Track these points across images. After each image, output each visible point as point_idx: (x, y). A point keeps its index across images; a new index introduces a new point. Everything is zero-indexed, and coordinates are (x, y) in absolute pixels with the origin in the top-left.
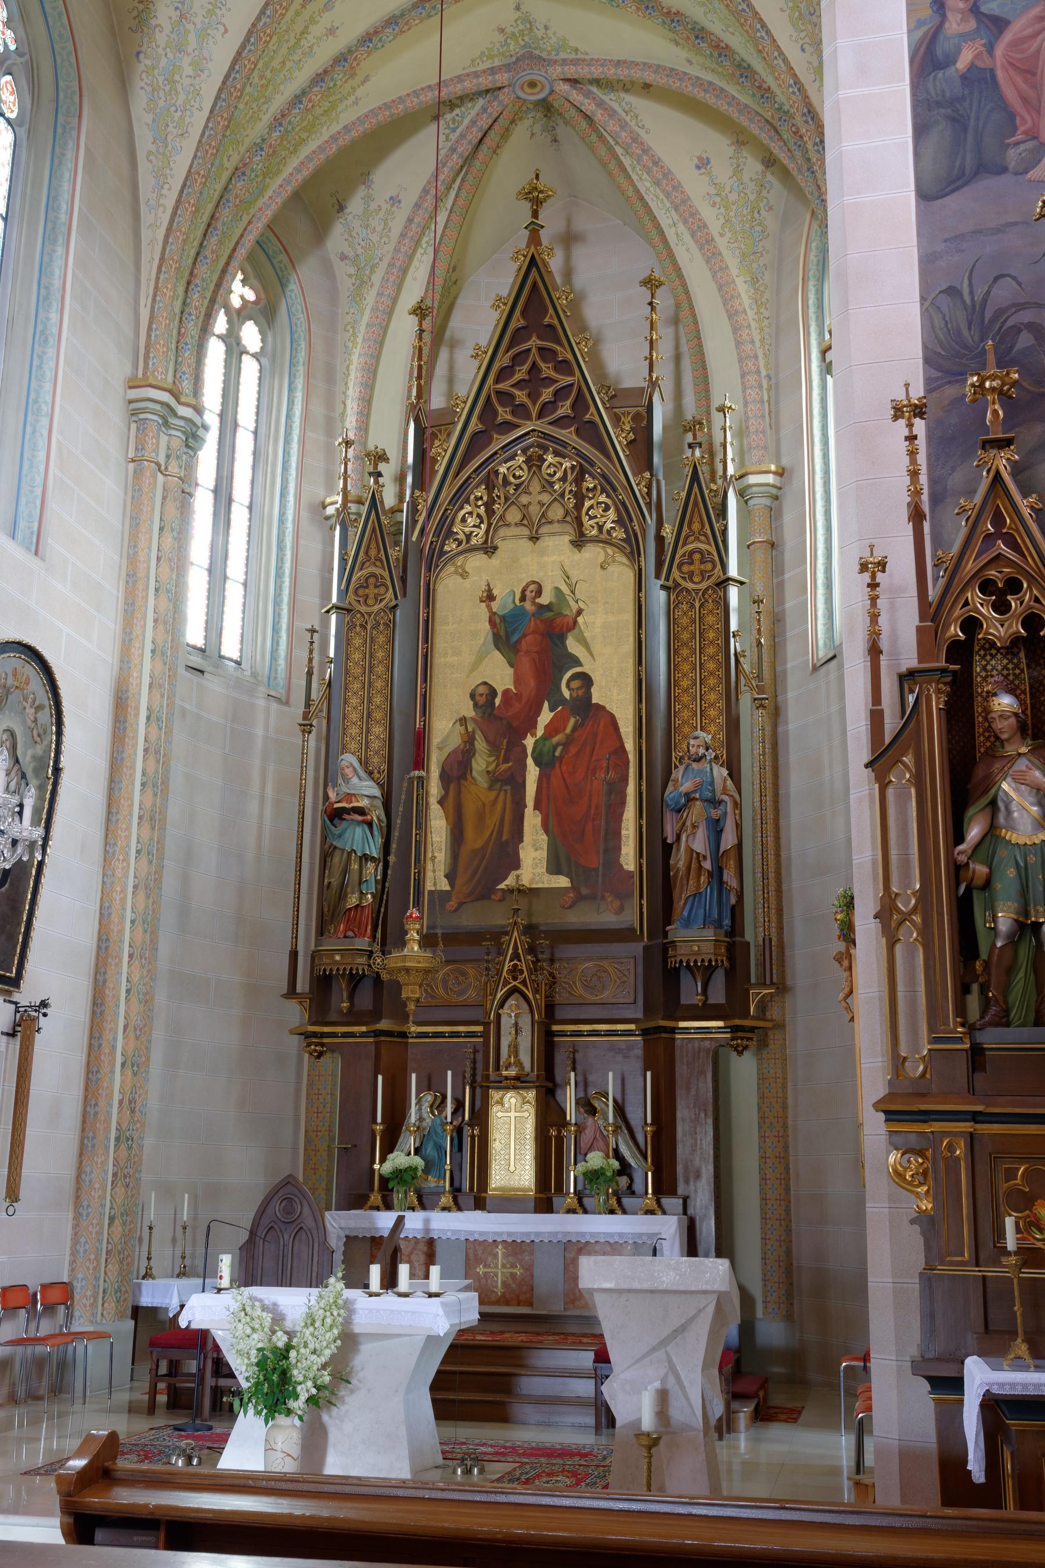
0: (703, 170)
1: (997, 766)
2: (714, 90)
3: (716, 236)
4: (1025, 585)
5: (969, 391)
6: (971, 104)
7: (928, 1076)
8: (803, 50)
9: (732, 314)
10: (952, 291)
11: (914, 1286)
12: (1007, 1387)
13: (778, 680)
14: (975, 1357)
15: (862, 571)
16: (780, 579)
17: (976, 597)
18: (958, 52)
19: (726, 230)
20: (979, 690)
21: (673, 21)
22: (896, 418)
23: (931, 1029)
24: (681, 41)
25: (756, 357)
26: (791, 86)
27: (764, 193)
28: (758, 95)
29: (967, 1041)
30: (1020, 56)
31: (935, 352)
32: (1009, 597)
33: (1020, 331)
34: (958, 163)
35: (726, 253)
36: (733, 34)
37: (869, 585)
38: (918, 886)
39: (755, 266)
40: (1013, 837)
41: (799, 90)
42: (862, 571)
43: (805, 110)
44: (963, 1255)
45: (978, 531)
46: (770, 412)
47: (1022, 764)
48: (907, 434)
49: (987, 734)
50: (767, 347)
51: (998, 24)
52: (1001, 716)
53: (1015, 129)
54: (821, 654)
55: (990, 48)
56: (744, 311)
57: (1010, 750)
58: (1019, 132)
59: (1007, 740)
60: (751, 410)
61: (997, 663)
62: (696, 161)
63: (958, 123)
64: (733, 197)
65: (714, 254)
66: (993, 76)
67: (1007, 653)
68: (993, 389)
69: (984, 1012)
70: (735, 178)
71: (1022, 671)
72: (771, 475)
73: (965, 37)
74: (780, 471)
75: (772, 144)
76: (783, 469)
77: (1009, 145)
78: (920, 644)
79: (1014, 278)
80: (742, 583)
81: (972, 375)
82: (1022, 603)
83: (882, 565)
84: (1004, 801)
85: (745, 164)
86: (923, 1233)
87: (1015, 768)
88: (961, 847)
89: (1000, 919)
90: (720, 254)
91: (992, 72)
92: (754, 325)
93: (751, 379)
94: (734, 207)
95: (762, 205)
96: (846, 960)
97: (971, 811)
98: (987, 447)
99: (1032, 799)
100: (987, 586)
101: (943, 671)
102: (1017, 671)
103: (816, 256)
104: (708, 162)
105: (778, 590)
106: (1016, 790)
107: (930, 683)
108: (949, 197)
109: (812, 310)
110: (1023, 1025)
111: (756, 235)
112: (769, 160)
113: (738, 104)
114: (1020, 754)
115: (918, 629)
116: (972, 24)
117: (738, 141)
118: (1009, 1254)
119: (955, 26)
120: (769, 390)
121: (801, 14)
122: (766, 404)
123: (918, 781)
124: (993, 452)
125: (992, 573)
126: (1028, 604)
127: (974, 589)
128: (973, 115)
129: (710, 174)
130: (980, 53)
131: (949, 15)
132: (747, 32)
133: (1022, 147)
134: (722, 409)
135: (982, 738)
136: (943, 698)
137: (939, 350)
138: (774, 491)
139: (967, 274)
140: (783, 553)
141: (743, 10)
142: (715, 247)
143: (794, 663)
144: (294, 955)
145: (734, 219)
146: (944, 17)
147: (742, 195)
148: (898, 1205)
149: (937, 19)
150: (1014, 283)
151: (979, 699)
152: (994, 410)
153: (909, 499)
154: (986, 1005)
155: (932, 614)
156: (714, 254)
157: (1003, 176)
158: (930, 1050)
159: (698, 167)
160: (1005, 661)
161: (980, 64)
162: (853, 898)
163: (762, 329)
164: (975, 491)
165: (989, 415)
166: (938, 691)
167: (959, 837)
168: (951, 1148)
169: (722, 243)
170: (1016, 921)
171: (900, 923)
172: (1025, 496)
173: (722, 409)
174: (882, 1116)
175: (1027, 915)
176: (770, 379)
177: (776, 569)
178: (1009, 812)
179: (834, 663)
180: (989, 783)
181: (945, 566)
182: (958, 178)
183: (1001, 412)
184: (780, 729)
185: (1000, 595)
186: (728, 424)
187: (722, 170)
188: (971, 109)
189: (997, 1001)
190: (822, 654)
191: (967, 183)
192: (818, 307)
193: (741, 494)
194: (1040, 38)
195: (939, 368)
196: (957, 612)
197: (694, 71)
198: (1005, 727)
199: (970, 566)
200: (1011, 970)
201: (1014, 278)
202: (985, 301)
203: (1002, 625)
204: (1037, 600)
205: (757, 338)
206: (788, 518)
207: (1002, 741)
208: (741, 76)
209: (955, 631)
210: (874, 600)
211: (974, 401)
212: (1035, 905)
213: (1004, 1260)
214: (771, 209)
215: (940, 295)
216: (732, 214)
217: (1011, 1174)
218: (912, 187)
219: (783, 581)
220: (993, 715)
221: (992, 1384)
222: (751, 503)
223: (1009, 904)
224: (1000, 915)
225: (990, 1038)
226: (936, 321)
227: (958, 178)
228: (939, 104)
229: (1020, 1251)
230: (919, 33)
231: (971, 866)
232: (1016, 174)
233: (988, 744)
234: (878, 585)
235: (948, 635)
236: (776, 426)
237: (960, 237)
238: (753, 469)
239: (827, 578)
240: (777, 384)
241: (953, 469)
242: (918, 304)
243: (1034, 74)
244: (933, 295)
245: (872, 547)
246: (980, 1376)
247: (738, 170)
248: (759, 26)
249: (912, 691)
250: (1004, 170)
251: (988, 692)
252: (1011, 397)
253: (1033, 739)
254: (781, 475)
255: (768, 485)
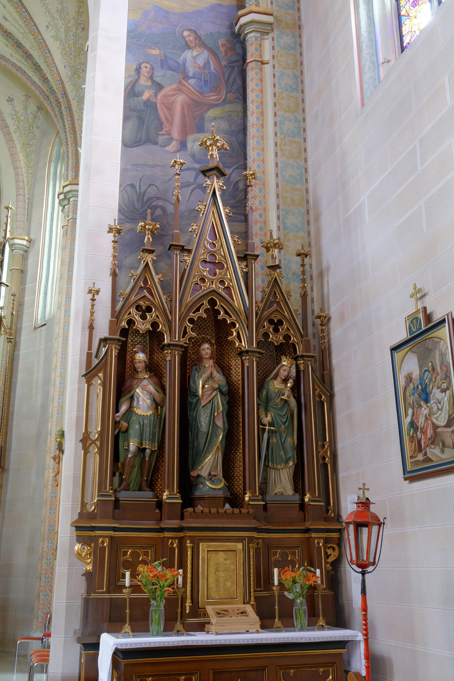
0: (10, 103)
1: (135, 382)
2: (21, 71)
3: (12, 133)
4: (153, 310)
5: (139, 228)
6: (146, 114)
7: (96, 511)
8: (65, 68)
9: (15, 168)
10: (132, 186)
11: (79, 603)
12: (143, 644)
13: (18, 331)
14: (106, 633)
15: (89, 293)
16: (24, 287)
17: (133, 311)
18: (144, 92)
19: (17, 131)
20: (129, 350)
21: (7, 36)
22: (109, 232)
23: (99, 491)
24: (9, 45)
25: (24, 189)
26: (58, 80)
27: (36, 120)
28: (42, 79)
29: (113, 496)
30: (167, 101)
31: (123, 209)
32: (147, 314)
33: (157, 208)
34: (139, 136)
35: (15, 140)
36: (34, 50)
37: (91, 299)
38: (99, 429)
39: (28, 150)
40: (139, 412)
41: (61, 83)
42: (89, 293)
43: (63, 92)
44: (103, 589)
45: (137, 285)
46: (28, 214)
47: (145, 382)
48: (113, 240)
49: (130, 368)
50: (29, 186)
51: (160, 87)
52: (139, 362)
53: (162, 129)
54: (39, 322)
55: (156, 95)
56: (21, 168)
57: (141, 376)
58: (164, 131)
59: (140, 372)
60: (19, 211)
61: (138, 339)
62: (7, 98)
63: (141, 120)
64: (22, 118)
65: (10, 140)
66: (156, 106)
67: (142, 336)
68: (149, 229)
69: (120, 485)
70: (24, 110)
71: (147, 344)
72: (25, 241)
73: (147, 87)
74: (29, 240)
75: (45, 102)
76: (31, 240)
77: (159, 134)
78: (110, 327)
79: (157, 187)
80: (7, 286)
81: (142, 222)
82: (151, 317)
83: (98, 292)
84: (137, 397)
85: (29, 106)
86: (86, 580)
87: (142, 383)
88: (117, 414)
89: (131, 446)
90: (13, 141)
91: (156, 104)
92: (25, 175)
93: (21, 197)
94: (22, 123)
95: (34, 125)
96: (58, 459)
97: (122, 400)
98: (144, 251)
99: (148, 397)
100: (138, 308)
101: (119, 340)
102: (145, 344)
103: (56, 153)
104: (13, 100)
105: (22, 291)
106: (142, 393)
107: (113, 344)
108: (134, 148)
109: (51, 175)
110: (134, 490)
111: (30, 137)
112: (40, 107)
113: (31, 80)
114: (145, 378)
115: (110, 321)
116: (150, 83)
117: (27, 95)
118: (126, 588)
119: (143, 81)
120: (29, 204)
121: (66, 52)
122: (26, 210)
123: (104, 384)
124: (147, 254)
125: (141, 303)
126: (154, 318)
127: (133, 308)
128: (147, 118)
129: (13, 105)
130: (152, 95)
131: (141, 77)
132: (42, 52)
133: (164, 137)
134: (7, 208)
135: (128, 370)
136: (117, 351)
137: (125, 208)
138: (25, 248)
139: (139, 181)
140: (26, 276)
141: (41, 42)
142: (11, 137)
143: (26, 325)
144: (2, 447)
145: (21, 128)
146: (139, 76)
147: (26, 118)
148: (72, 568)
149: (136, 77)
150: (156, 189)
151: (129, 353)
152: (148, 238)
153: (111, 267)
154: (121, 481)
155: (116, 316)
156: (10, 140)
157: (156, 146)
158: (98, 500)
159: (8, 101)
160: (141, 339)
161: (151, 100)
162: (64, 432)
163: (28, 178)
164: (138, 268)
165: (146, 239)
166: (178, 354)
167: (117, 411)
168: (103, 542)
169: (15, 136)
170: (137, 447)
171: (90, 445)
172: (157, 274)
173: (7, 208)
174: (74, 529)
175: (141, 444)
176: (29, 199)
177: (23, 282)
178: (138, 401)
179: (44, 327)
180: (131, 389)
181: (123, 296)
182: (139, 142)
183: (151, 239)
184: (16, 353)
185: (144, 312)
186: (9, 215)
187: (19, 105)
188: (146, 116)
189: (126, 480)
190: (39, 323)
191: (142, 145)
192: (54, 175)
193: (11, 246)
194: (175, 97)
195: (124, 215)
196: (126, 317)
197: (13, 60)
198: (140, 366)
199: (133, 299)
200: (133, 467)
201: (157, 187)
202: (144, 193)
203: (143, 325)
204: (157, 317)
205: (26, 181)
206: (30, 261)
207: (138, 372)
208: (36, 69)
209: (124, 324)
210: (93, 306)
211: (140, 232)
212: (145, 441)
213: (124, 591)
214: (38, 128)
215: (126, 186)
216: (21, 125)
217: (125, 553)
218: (121, 140)
219: (25, 288)
220: (136, 361)
221: (117, 645)
222: (14, 251)
223: (135, 439)
224: (131, 444)
225: (123, 496)
226: (125, 196)
227: (139, 142)
228: (134, 110)
229: (131, 586)
230: (129, 80)
231: (121, 422)
232: (161, 146)
233: (131, 372)
234: (95, 300)
235: (121, 325)
236: (29, 220)
237: (138, 165)
238: (18, 237)
239: (45, 290)
240: (32, 203)
241: (126, 257)
242: (118, 188)
243: (171, 110)
244: (125, 185)
245: (94, 283)
246: (108, 643)
247: (26, 107)
248: (47, 51)
249: (105, 347)
250: (156, 143)
251: (135, 351)
252: (155, 234)
253: (150, 372)
254: (30, 242)
255: (23, 245)
